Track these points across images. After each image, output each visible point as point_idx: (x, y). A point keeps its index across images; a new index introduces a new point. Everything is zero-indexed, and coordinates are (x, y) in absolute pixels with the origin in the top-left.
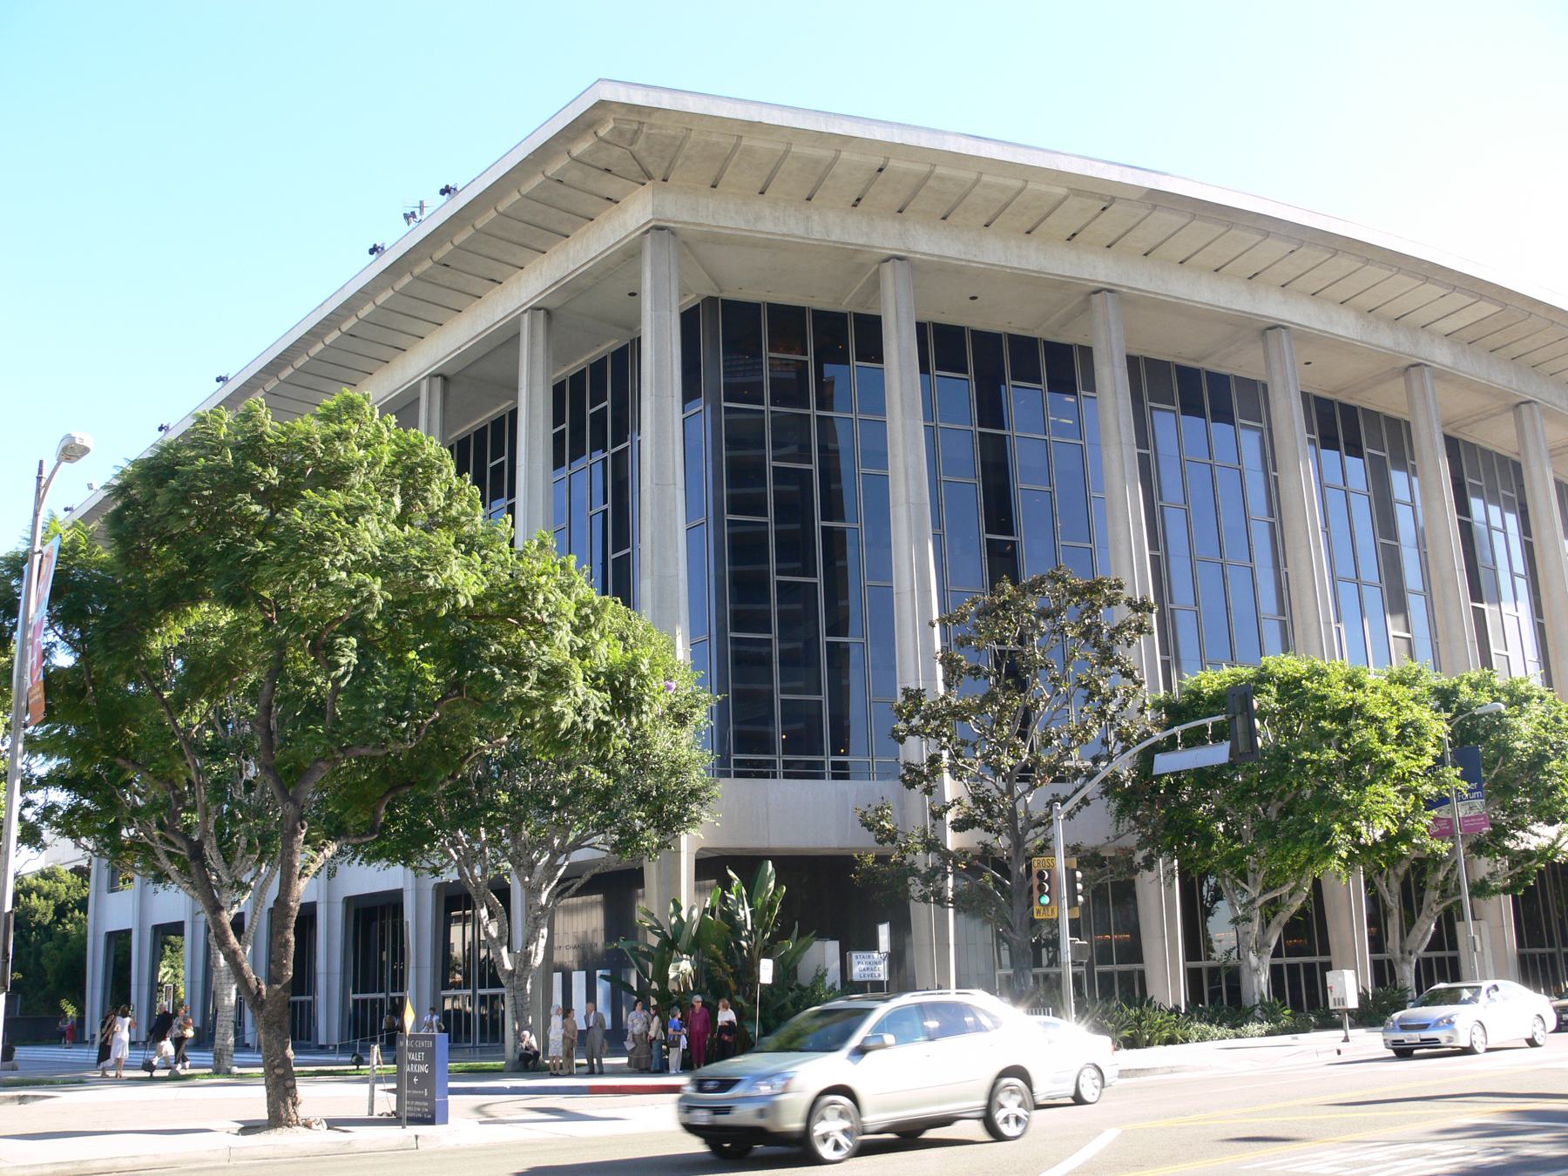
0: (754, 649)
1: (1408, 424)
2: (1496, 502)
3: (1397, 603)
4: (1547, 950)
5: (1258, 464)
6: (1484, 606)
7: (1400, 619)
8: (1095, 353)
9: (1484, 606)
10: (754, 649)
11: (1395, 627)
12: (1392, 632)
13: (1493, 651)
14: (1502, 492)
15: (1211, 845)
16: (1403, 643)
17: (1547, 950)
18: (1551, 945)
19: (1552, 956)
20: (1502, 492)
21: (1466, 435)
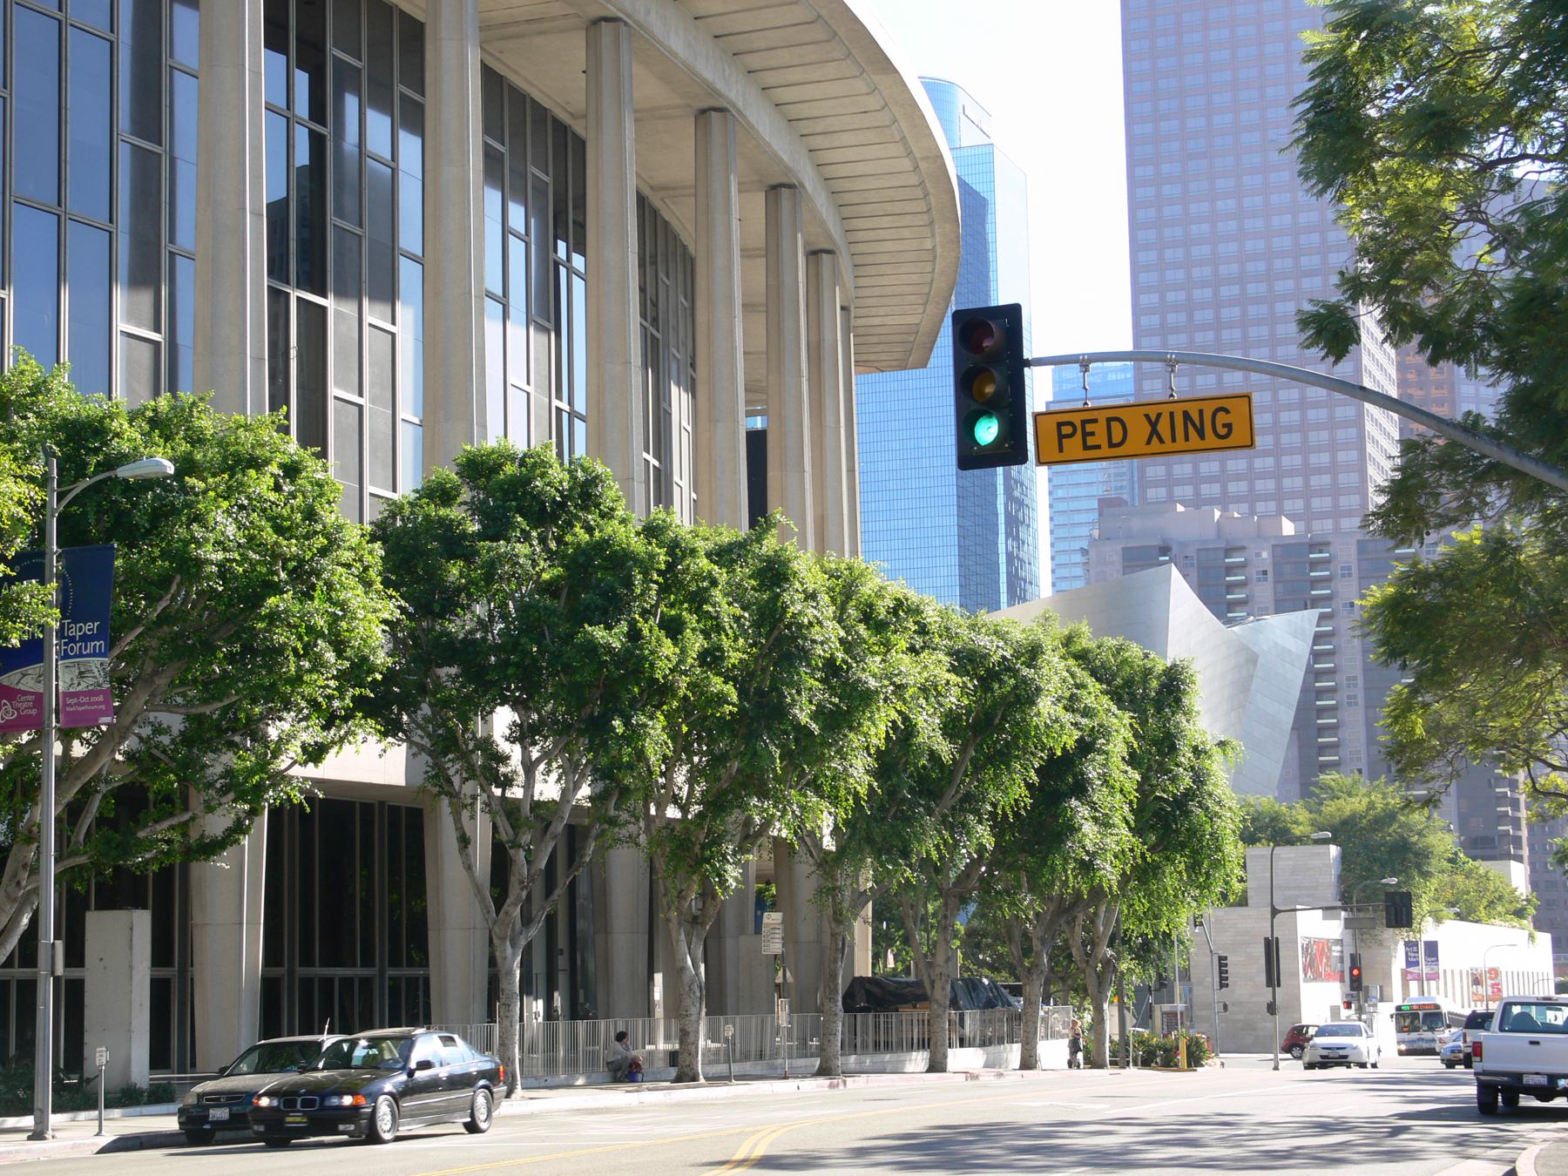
0: (421, 993)
1: (581, 144)
2: (384, 105)
3: (149, 269)
4: (358, 971)
5: (403, 181)
6: (329, 302)
7: (145, 298)
8: (953, 460)
9: (329, 302)
10: (421, 993)
11: (131, 317)
12: (121, 325)
13: (333, 391)
14: (399, 88)
15: (1085, 1058)
16: (145, 352)
17: (358, 971)
18: (368, 961)
19: (366, 982)
20: (399, 88)
21: (655, 199)
